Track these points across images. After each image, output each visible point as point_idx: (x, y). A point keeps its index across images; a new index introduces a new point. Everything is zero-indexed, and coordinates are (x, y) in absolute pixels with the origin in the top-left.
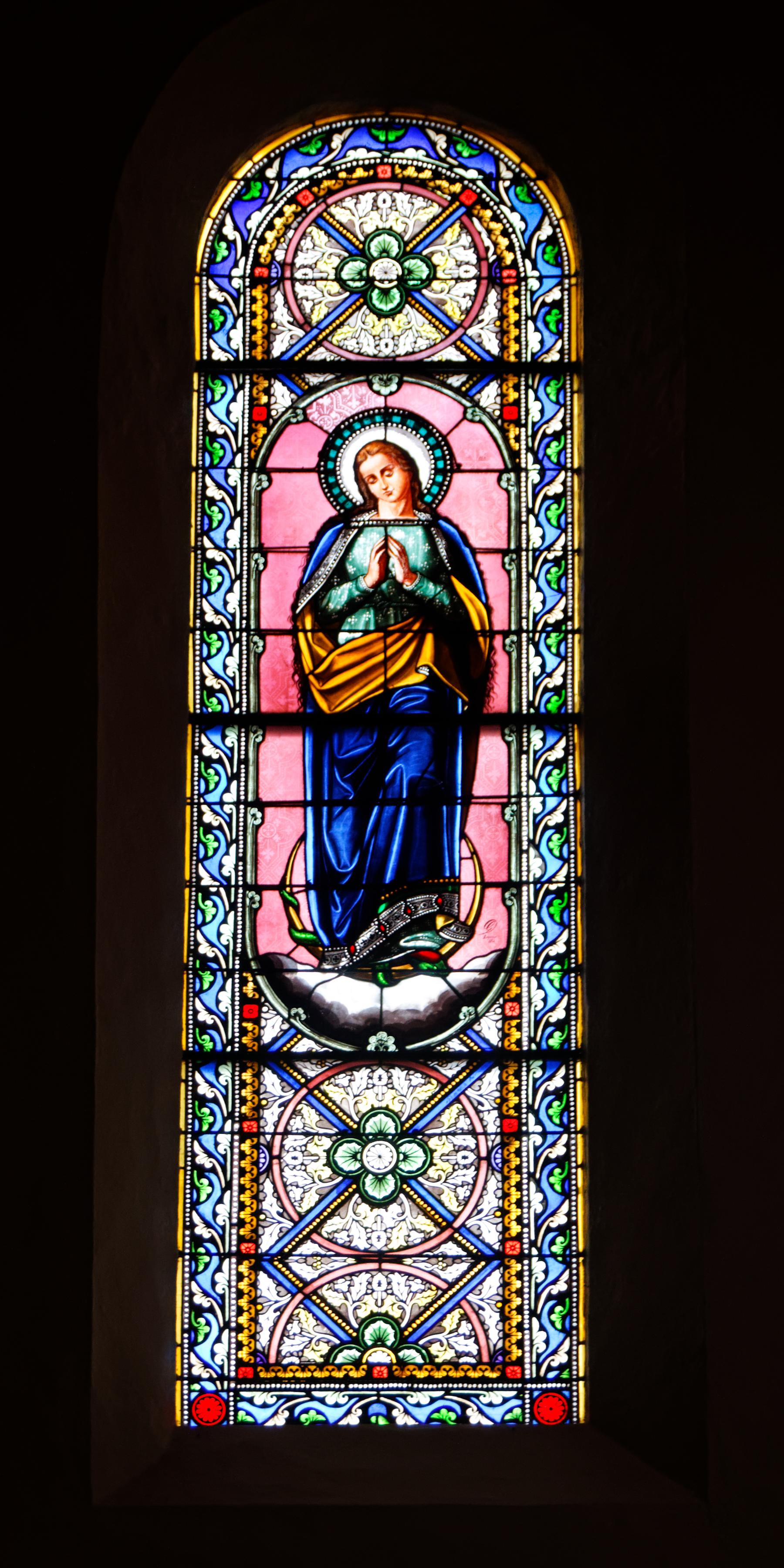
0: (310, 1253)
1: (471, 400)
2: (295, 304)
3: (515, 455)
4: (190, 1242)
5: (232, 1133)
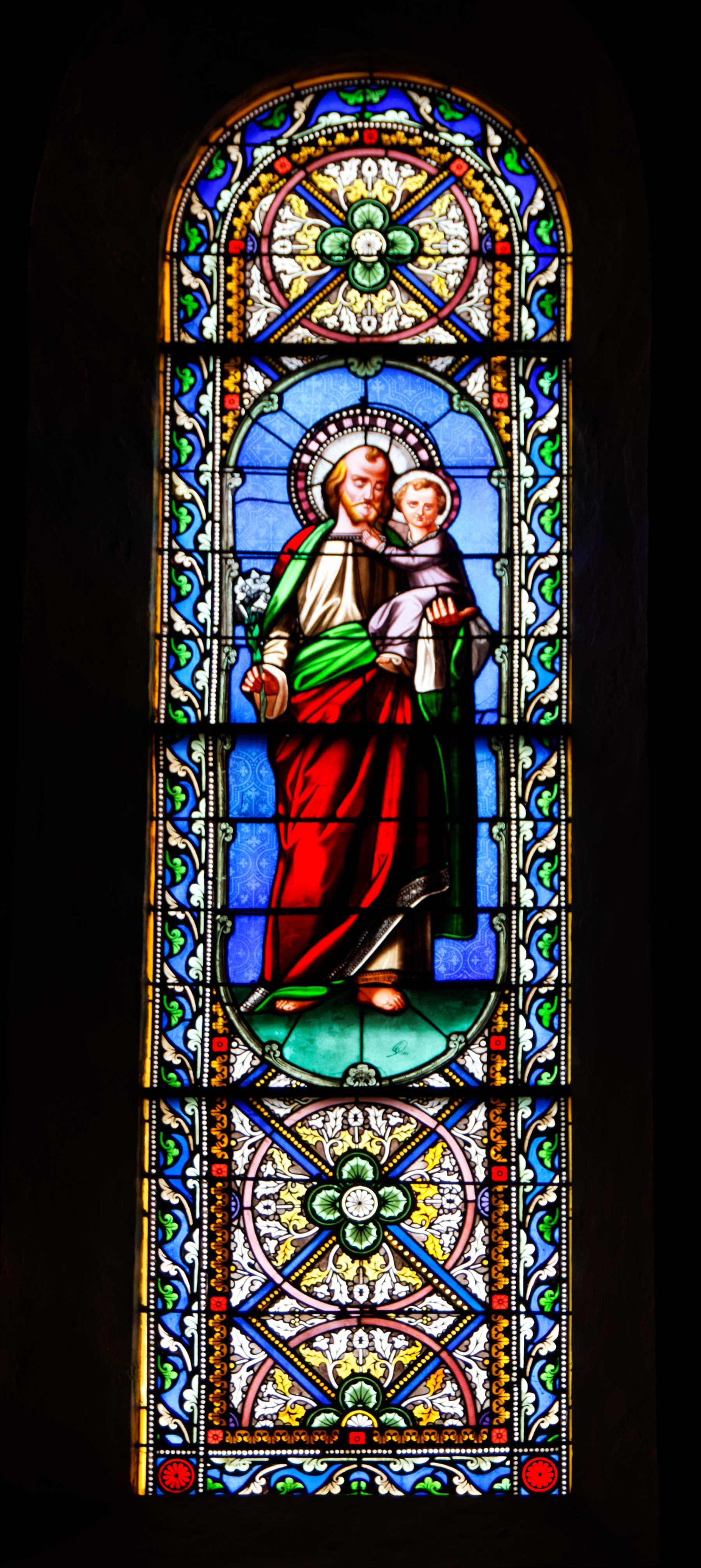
0: (287, 1310)
1: (457, 385)
2: (272, 279)
3: (506, 447)
4: (157, 1208)
5: (218, 254)
